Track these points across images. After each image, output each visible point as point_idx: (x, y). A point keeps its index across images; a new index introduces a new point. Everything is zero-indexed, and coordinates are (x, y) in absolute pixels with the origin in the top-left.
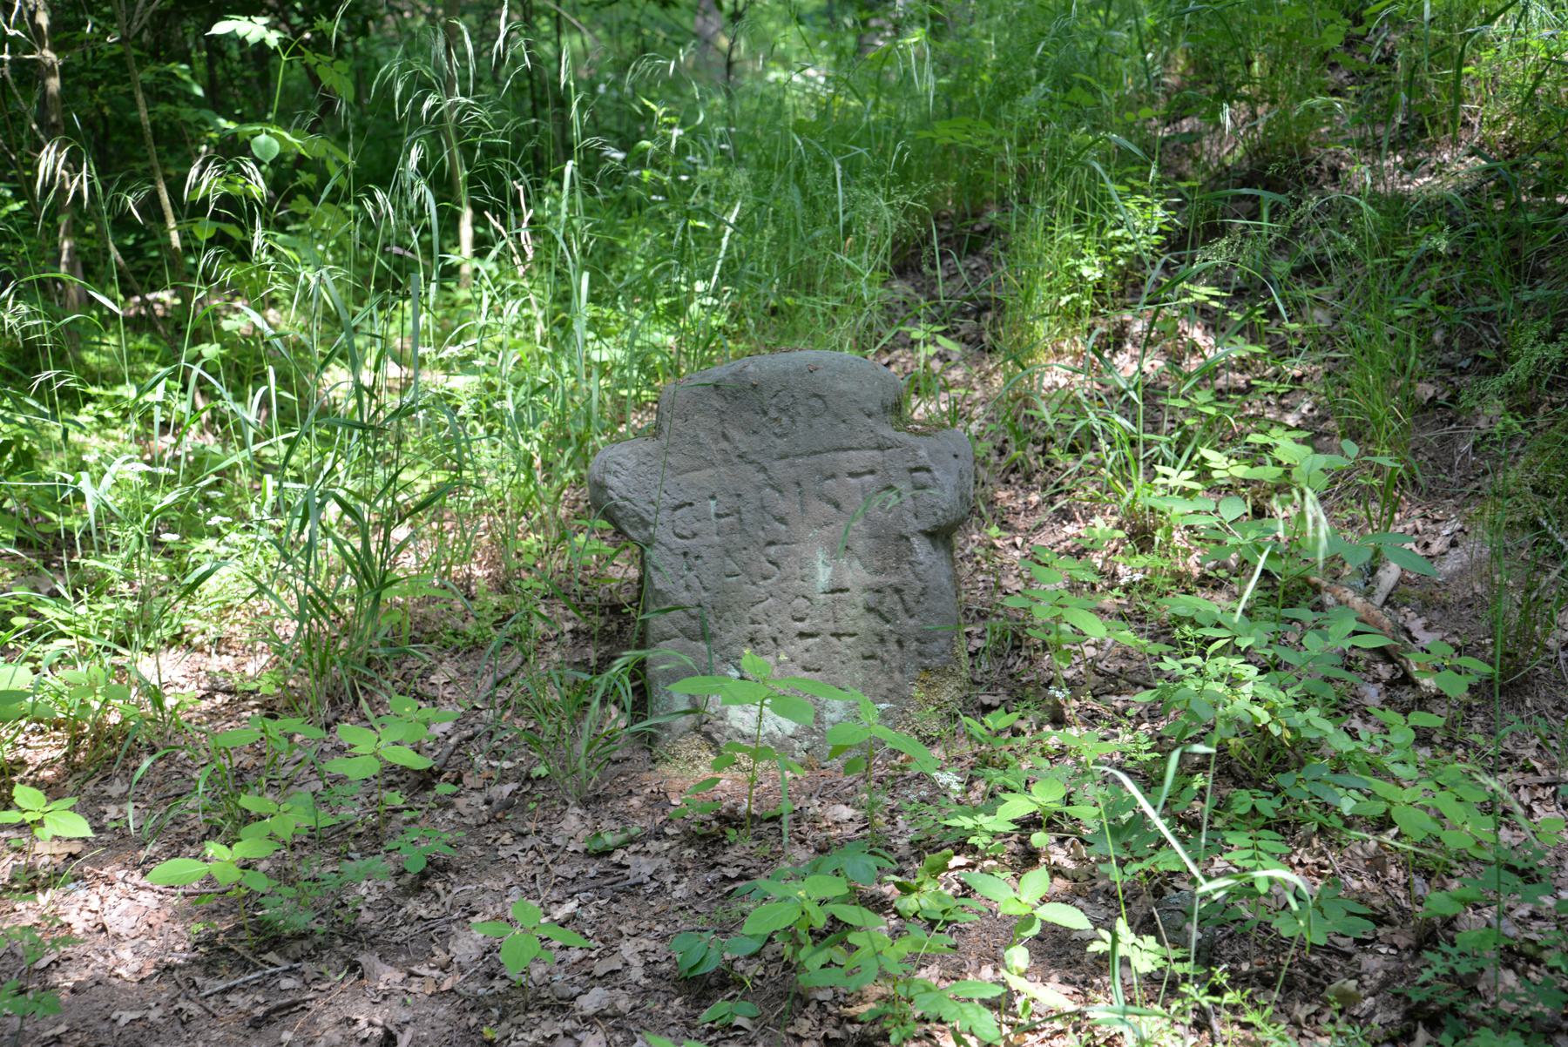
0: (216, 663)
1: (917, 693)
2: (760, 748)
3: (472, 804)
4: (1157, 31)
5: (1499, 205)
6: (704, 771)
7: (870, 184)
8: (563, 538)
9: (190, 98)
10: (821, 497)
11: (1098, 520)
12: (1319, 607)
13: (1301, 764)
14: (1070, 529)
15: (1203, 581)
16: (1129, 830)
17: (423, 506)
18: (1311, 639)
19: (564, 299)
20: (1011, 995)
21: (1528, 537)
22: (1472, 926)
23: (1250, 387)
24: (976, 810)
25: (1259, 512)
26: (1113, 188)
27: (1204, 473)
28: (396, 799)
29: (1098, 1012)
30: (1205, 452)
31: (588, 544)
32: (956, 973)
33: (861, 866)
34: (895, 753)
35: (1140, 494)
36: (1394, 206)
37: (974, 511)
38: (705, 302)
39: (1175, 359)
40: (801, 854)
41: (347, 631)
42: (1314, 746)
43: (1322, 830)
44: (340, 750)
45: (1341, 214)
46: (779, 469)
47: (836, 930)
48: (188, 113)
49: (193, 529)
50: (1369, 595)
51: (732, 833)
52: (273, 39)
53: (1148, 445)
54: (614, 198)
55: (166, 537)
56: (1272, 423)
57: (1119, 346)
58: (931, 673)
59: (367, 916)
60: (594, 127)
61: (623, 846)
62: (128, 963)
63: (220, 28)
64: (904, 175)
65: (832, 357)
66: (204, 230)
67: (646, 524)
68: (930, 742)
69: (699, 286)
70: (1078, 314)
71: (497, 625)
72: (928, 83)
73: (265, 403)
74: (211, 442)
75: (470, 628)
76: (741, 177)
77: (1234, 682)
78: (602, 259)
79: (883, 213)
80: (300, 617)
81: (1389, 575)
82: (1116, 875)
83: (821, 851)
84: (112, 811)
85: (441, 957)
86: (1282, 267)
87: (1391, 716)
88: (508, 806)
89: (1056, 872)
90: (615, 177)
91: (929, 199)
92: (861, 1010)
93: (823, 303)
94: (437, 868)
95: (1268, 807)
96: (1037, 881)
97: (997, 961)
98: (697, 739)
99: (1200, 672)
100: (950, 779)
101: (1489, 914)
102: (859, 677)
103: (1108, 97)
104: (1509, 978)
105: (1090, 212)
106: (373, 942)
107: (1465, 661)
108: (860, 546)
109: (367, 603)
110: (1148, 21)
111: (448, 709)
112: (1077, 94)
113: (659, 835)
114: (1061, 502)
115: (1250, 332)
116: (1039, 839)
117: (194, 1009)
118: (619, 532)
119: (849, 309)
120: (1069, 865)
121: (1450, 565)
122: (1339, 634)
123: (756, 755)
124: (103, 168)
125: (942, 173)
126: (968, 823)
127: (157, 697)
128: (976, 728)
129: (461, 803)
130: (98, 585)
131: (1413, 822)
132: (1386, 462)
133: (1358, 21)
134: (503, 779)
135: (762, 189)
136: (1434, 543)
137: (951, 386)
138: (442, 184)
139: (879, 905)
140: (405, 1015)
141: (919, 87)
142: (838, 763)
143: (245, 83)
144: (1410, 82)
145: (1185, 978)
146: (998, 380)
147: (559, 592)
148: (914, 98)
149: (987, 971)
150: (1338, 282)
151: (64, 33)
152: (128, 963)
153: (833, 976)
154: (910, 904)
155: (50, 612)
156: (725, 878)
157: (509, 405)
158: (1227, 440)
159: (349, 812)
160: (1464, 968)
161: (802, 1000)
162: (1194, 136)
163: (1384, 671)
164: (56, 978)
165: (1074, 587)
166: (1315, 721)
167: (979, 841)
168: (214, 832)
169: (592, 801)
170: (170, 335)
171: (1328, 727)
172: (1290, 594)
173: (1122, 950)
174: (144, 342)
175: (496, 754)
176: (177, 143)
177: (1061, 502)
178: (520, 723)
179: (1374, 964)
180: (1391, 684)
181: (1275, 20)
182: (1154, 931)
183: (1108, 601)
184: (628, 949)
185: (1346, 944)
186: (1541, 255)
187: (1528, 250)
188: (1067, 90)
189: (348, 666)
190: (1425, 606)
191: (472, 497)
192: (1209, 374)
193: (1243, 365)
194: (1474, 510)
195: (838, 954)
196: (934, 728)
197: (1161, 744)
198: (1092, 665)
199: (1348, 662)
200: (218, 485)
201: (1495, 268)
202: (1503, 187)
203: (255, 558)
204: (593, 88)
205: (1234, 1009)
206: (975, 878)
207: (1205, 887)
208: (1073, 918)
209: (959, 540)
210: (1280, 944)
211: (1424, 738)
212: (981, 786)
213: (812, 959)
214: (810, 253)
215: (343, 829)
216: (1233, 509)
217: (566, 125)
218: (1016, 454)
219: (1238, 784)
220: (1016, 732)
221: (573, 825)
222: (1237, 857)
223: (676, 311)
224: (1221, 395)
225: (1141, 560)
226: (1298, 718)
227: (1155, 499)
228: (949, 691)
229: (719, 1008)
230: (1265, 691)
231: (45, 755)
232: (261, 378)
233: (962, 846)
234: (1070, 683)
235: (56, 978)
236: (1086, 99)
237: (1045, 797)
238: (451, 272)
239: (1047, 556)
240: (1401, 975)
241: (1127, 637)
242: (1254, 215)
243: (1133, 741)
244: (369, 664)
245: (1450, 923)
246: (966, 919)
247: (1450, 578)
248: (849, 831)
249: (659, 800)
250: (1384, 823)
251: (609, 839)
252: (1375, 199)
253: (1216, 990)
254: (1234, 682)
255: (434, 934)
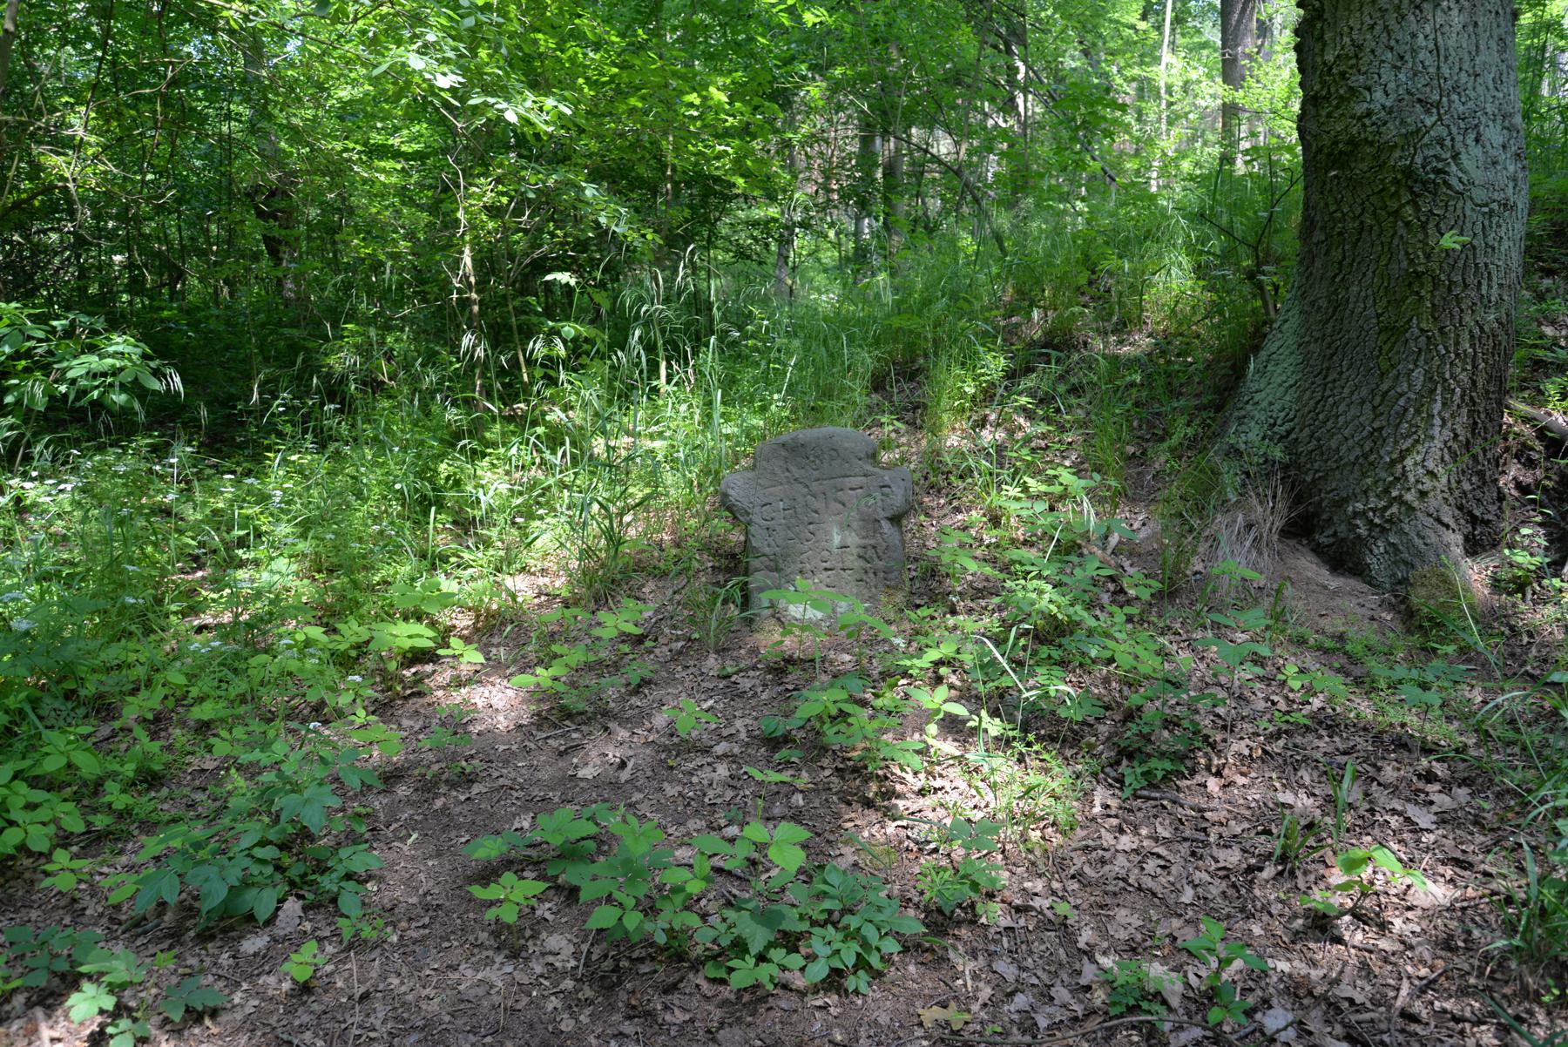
0: (542, 581)
1: (883, 598)
2: (805, 626)
3: (662, 652)
4: (998, 275)
5: (1162, 361)
6: (777, 637)
7: (860, 346)
8: (707, 520)
9: (537, 313)
10: (836, 500)
11: (974, 513)
12: (1081, 555)
13: (1072, 633)
14: (960, 517)
15: (1025, 543)
16: (989, 667)
17: (638, 505)
18: (1077, 571)
19: (709, 404)
20: (928, 747)
21: (1177, 521)
22: (1150, 710)
23: (1047, 447)
24: (912, 657)
25: (1052, 509)
26: (981, 349)
27: (1025, 489)
28: (626, 648)
29: (971, 756)
30: (1026, 478)
31: (720, 524)
32: (902, 737)
33: (855, 685)
34: (872, 628)
35: (994, 499)
36: (1114, 360)
37: (912, 507)
38: (778, 403)
39: (1011, 432)
40: (824, 678)
41: (603, 566)
42: (1078, 624)
43: (1081, 665)
44: (599, 624)
45: (1089, 364)
46: (815, 486)
47: (842, 715)
48: (534, 319)
49: (530, 516)
50: (1104, 549)
51: (790, 668)
52: (573, 282)
53: (998, 475)
54: (733, 353)
55: (518, 520)
56: (1059, 465)
57: (983, 426)
58: (891, 588)
59: (612, 705)
60: (724, 318)
61: (736, 673)
62: (502, 723)
63: (549, 277)
64: (877, 342)
65: (841, 430)
66: (539, 372)
67: (748, 514)
68: (890, 623)
69: (776, 396)
70: (963, 410)
71: (675, 564)
72: (888, 298)
73: (564, 455)
74: (540, 475)
75: (662, 565)
76: (796, 343)
77: (1041, 592)
78: (729, 383)
79: (867, 360)
80: (580, 559)
81: (1114, 540)
82: (981, 688)
83: (835, 676)
84: (494, 650)
85: (648, 725)
86: (1062, 388)
87: (1115, 609)
88: (680, 653)
89: (951, 687)
90: (735, 343)
91: (890, 353)
92: (855, 754)
93: (837, 404)
94: (646, 682)
95: (1056, 654)
96: (942, 692)
97: (922, 731)
98: (774, 621)
99: (1024, 588)
100: (900, 642)
101: (1157, 703)
102: (855, 590)
103: (977, 305)
104: (1166, 733)
105: (969, 360)
106: (615, 717)
107: (1150, 582)
108: (855, 525)
109: (612, 552)
110: (994, 270)
111: (651, 605)
112: (961, 303)
113: (754, 668)
114: (955, 503)
115: (1047, 420)
116: (943, 671)
117: (533, 746)
118: (735, 518)
119: (851, 408)
120: (958, 683)
121: (1142, 534)
122: (1091, 569)
123: (803, 629)
124: (494, 346)
125: (896, 341)
126: (908, 663)
127: (514, 597)
128: (913, 616)
129: (657, 651)
130: (487, 543)
131: (1125, 660)
132: (1113, 483)
133: (1093, 272)
134: (678, 640)
135: (806, 349)
136: (1137, 523)
137: (900, 445)
138: (650, 348)
139: (863, 703)
140: (631, 753)
141: (884, 300)
142: (843, 633)
143: (560, 304)
144: (1119, 303)
145: (1014, 738)
146: (924, 443)
147: (705, 547)
148: (882, 305)
149: (917, 736)
150: (1088, 396)
151: (481, 286)
152: (502, 723)
153: (841, 738)
154: (879, 703)
155: (466, 555)
156: (787, 690)
157: (681, 455)
158: (1036, 473)
159: (603, 655)
160: (1146, 730)
161: (824, 749)
162: (1018, 325)
163: (1111, 586)
164: (471, 728)
165: (962, 545)
166: (1079, 612)
167: (913, 672)
168: (540, 662)
169: (721, 651)
170: (520, 423)
171: (1085, 614)
172: (1069, 549)
173: (984, 725)
174: (512, 427)
175: (674, 627)
176: (528, 333)
177: (955, 503)
178: (686, 613)
179: (1103, 729)
180: (1114, 593)
181: (1055, 271)
182: (999, 716)
183: (978, 553)
184: (739, 724)
185: (1091, 720)
186: (1181, 385)
187: (1176, 383)
188: (956, 301)
189: (604, 582)
190: (1130, 555)
191: (663, 500)
192: (1027, 440)
193: (1044, 436)
194: (1152, 508)
195: (842, 727)
196: (892, 616)
197: (1006, 625)
198: (970, 585)
199: (1095, 582)
200: (543, 495)
201: (1161, 390)
202: (1163, 353)
203: (559, 530)
204: (725, 302)
205: (1037, 752)
206: (911, 690)
207: (1026, 695)
208: (959, 710)
209: (905, 522)
210: (1060, 721)
211: (1130, 619)
212: (915, 644)
213: (829, 730)
214: (830, 379)
215: (600, 662)
216: (1041, 506)
217: (711, 319)
218: (933, 479)
219: (1041, 643)
220: (933, 618)
221: (712, 663)
222: (1041, 679)
223: (764, 409)
224: (1033, 450)
225: (995, 532)
226: (1071, 610)
227: (1002, 502)
228: (899, 598)
229: (784, 753)
230: (1055, 597)
231: (465, 623)
232: (563, 444)
233: (905, 674)
234: (960, 593)
235: (471, 728)
236: (966, 306)
237: (947, 650)
238: (655, 390)
239: (948, 530)
240: (1116, 734)
241: (988, 570)
242: (1048, 362)
243: (991, 622)
244: (613, 581)
245: (1139, 708)
246: (907, 711)
247: (1142, 541)
248: (849, 666)
249: (754, 651)
250: (1111, 661)
251: (730, 670)
252: (1104, 357)
253: (1029, 745)
254: (1041, 592)
255: (644, 715)
